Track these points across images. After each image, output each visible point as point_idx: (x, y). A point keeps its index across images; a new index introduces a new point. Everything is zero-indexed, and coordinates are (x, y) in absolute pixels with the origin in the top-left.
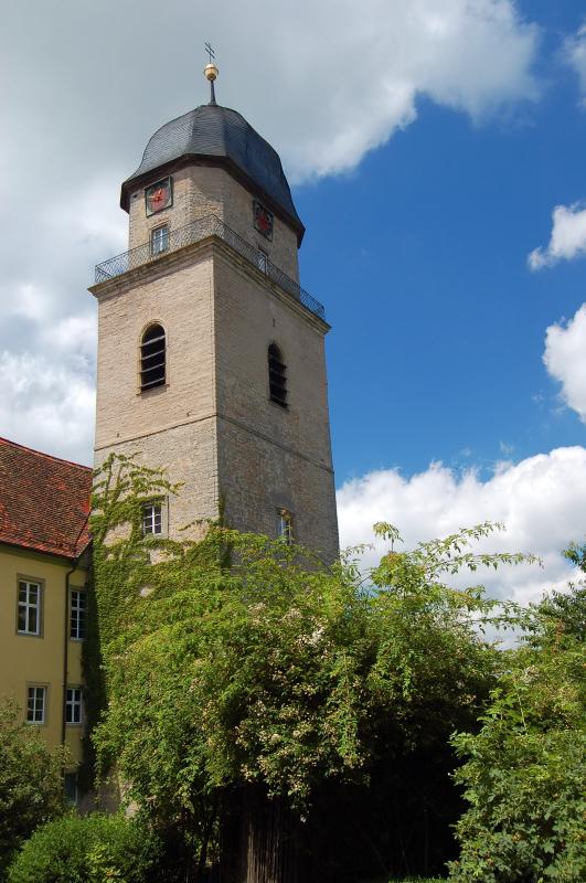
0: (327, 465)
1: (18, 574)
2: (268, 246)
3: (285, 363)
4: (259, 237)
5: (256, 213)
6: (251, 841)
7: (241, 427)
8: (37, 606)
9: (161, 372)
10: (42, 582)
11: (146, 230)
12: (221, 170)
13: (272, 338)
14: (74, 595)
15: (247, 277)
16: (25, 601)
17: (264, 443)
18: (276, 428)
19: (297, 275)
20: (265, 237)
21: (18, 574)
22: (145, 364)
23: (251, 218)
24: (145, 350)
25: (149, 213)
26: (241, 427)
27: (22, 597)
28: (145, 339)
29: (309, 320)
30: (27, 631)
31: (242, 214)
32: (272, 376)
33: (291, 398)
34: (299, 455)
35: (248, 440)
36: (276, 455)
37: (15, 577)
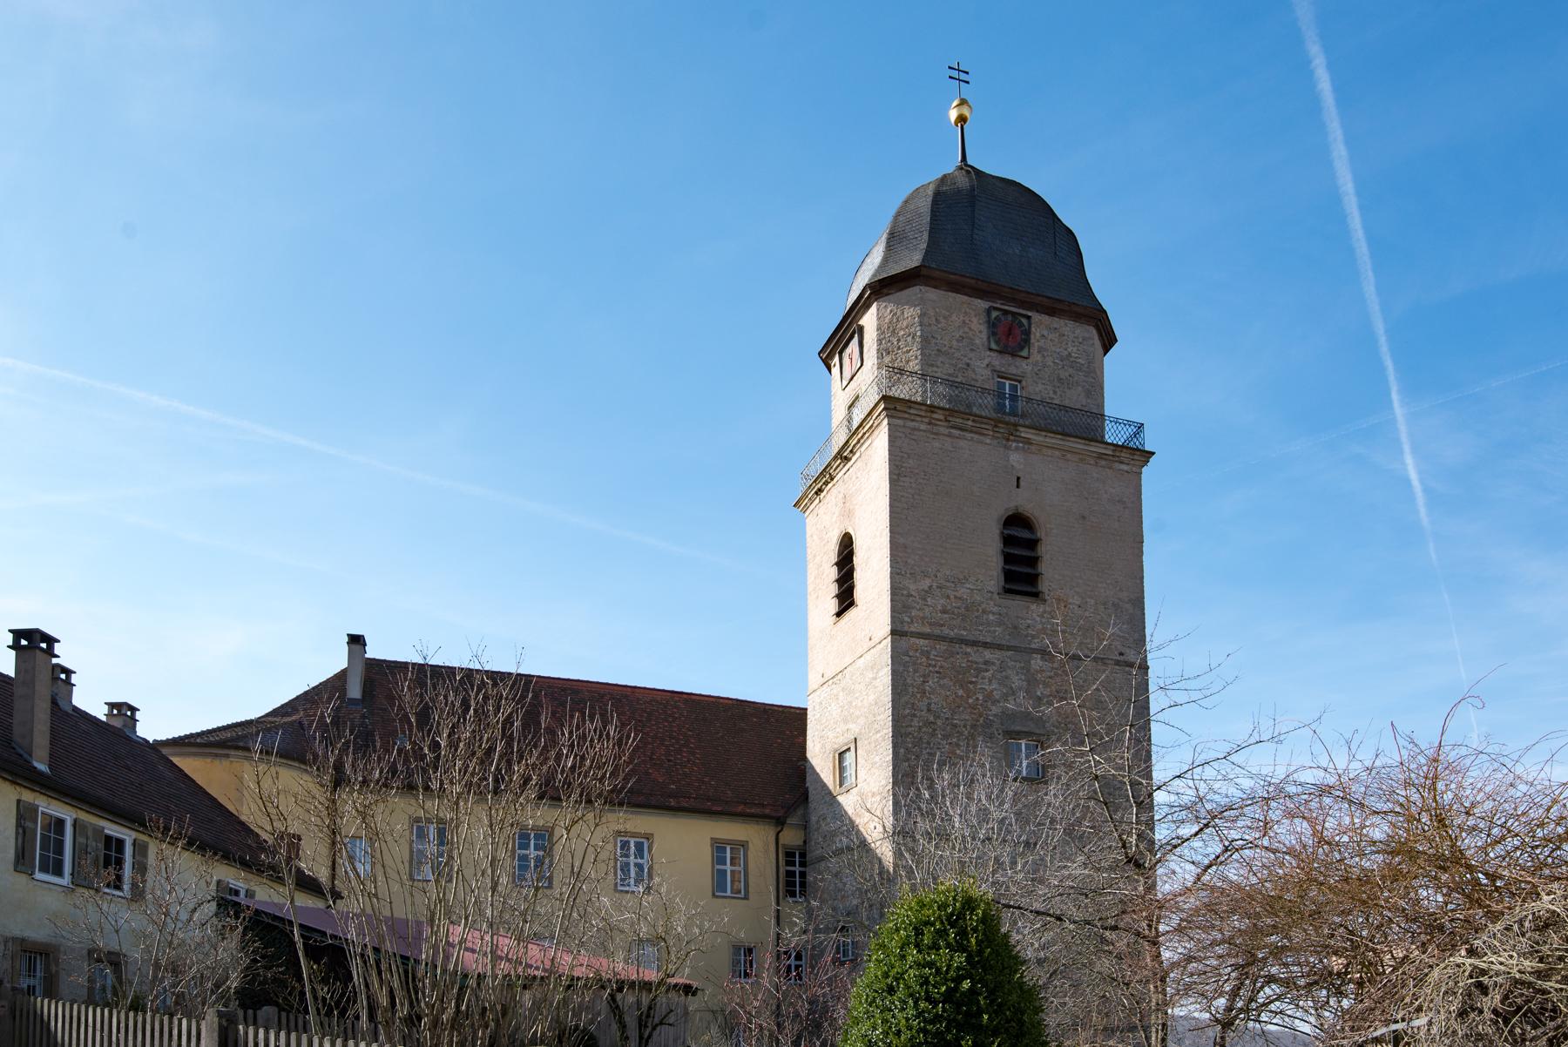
4: (998, 361)
12: (916, 289)
18: (1015, 627)
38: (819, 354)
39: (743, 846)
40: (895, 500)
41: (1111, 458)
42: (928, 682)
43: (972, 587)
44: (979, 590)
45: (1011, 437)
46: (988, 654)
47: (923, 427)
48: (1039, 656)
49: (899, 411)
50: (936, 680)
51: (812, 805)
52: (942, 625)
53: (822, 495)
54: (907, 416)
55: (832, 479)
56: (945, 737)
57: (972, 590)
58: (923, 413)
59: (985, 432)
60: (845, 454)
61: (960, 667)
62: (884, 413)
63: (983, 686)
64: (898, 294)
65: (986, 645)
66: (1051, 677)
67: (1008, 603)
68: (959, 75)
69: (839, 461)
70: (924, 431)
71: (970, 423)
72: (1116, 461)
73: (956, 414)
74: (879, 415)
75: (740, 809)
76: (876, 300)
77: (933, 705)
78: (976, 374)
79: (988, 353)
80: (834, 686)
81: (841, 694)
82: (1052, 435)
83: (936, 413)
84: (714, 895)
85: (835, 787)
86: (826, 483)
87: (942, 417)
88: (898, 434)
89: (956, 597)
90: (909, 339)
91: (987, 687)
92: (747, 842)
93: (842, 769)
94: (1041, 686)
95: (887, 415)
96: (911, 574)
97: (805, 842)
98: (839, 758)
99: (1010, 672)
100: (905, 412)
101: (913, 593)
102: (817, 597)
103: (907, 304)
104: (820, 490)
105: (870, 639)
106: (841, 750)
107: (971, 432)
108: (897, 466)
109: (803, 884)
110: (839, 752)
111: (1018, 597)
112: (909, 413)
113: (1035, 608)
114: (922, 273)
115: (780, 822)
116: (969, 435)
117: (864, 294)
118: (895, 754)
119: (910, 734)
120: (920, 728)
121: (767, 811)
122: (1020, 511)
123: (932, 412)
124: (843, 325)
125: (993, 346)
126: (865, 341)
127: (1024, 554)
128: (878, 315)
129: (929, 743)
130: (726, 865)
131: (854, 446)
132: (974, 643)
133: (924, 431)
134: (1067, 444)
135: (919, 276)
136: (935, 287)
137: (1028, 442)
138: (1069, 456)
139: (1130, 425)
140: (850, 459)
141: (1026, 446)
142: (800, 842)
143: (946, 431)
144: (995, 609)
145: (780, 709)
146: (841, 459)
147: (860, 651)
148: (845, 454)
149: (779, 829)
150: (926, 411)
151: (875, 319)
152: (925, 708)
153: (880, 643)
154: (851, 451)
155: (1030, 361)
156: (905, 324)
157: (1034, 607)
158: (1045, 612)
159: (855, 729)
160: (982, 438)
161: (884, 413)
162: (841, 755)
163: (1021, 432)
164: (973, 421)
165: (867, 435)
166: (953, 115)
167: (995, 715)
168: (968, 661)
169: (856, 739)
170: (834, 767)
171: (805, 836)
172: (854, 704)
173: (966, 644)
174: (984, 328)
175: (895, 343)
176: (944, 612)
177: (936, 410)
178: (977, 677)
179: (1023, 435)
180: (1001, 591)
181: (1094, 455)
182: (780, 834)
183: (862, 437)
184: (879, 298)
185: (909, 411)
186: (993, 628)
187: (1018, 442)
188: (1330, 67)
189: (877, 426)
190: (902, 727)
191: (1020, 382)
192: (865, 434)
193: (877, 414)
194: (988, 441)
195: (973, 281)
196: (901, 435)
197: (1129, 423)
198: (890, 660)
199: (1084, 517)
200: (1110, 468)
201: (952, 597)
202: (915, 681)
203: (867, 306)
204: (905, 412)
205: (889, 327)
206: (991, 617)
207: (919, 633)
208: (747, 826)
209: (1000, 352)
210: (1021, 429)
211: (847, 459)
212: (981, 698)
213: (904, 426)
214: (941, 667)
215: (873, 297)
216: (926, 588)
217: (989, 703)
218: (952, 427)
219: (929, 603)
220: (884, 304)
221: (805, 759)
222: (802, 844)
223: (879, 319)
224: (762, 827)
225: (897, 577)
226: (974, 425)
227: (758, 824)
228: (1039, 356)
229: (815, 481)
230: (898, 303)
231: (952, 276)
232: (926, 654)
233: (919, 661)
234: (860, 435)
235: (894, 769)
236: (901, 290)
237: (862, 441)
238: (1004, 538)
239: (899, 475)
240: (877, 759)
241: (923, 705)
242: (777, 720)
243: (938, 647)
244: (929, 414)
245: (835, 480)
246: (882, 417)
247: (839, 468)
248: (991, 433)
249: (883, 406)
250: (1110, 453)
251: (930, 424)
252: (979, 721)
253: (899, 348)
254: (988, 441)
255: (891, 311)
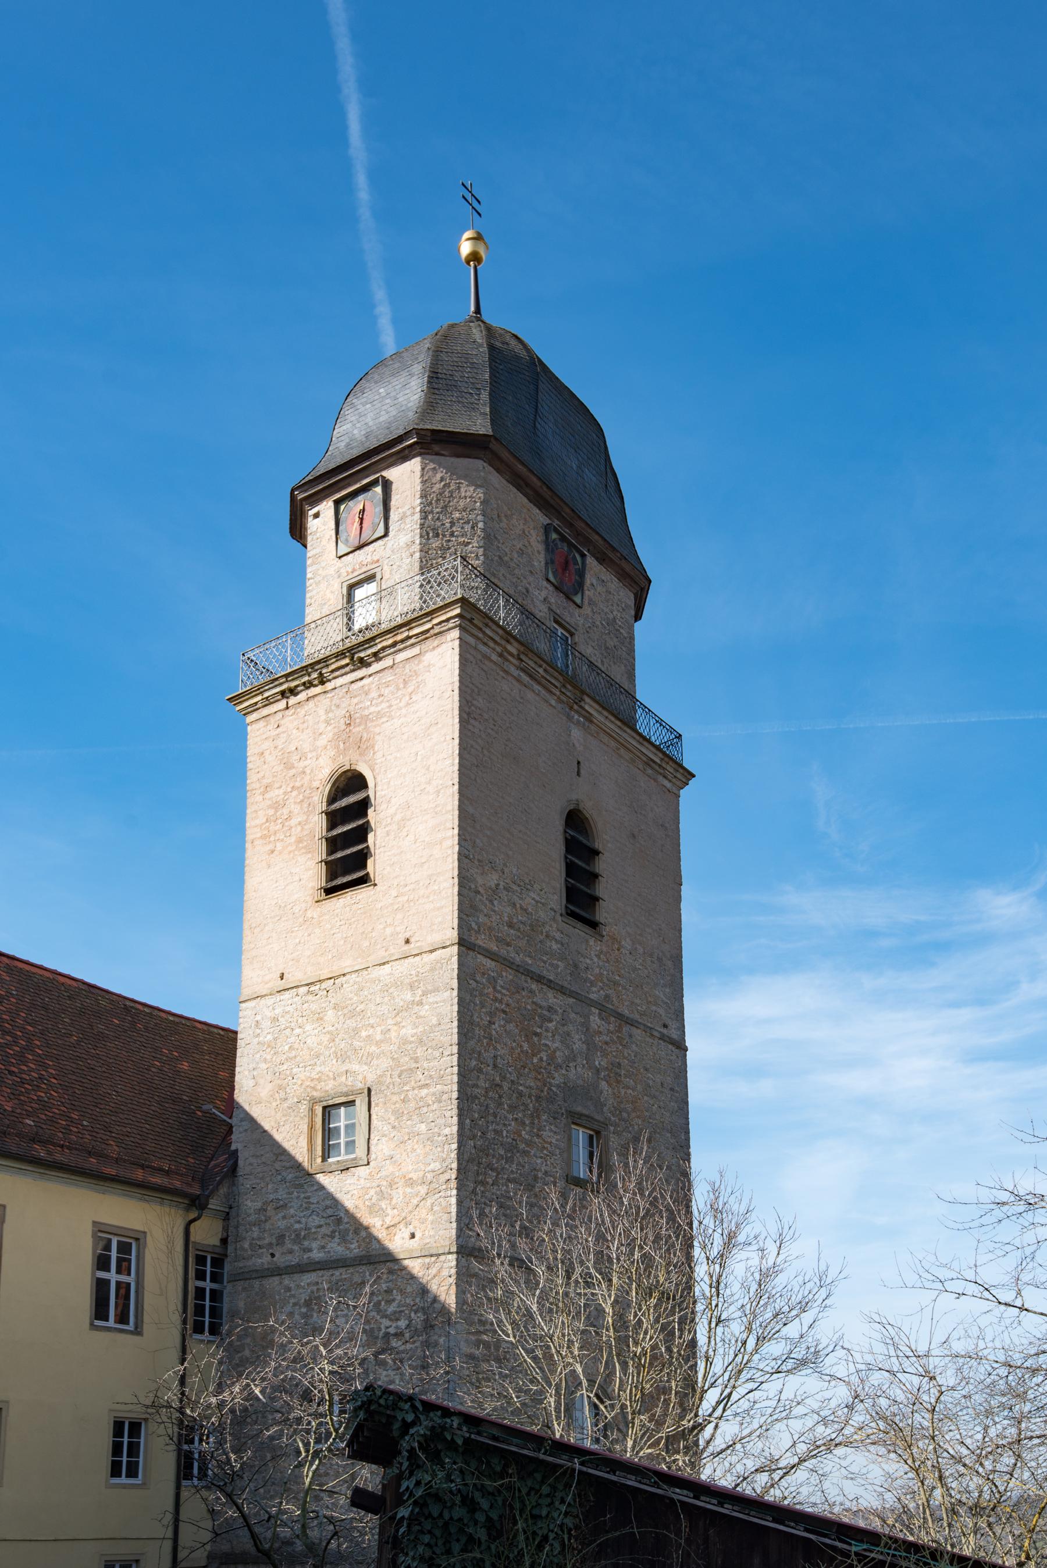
0: (674, 1035)
1: (94, 1222)
2: (574, 617)
3: (598, 845)
4: (556, 600)
5: (549, 547)
6: (380, 294)
7: (507, 963)
8: (131, 1279)
9: (361, 859)
10: (140, 1238)
11: (336, 585)
12: (479, 464)
13: (574, 797)
14: (201, 1260)
15: (525, 678)
16: (108, 1270)
17: (550, 994)
18: (576, 966)
19: (631, 676)
20: (568, 598)
21: (94, 1222)
22: (333, 844)
23: (539, 560)
24: (334, 818)
25: (343, 549)
26: (507, 963)
27: (102, 1263)
28: (332, 799)
29: (649, 762)
30: (111, 1323)
31: (521, 552)
32: (571, 870)
33: (603, 913)
34: (619, 1016)
35: (519, 989)
36: (573, 1015)
37: (89, 1229)
38: (293, 491)
39: (137, 1239)
40: (464, 749)
41: (657, 768)
42: (494, 1024)
43: (537, 898)
44: (543, 904)
45: (576, 707)
46: (552, 998)
47: (494, 657)
48: (597, 1011)
49: (476, 626)
50: (502, 1023)
51: (245, 1183)
52: (508, 944)
53: (293, 700)
54: (481, 635)
55: (322, 683)
56: (513, 1108)
57: (537, 902)
58: (497, 638)
59: (554, 690)
60: (362, 655)
61: (525, 1008)
62: (457, 621)
63: (547, 1042)
64: (453, 459)
65: (550, 984)
66: (606, 1043)
67: (569, 929)
68: (472, 200)
69: (347, 661)
70: (495, 663)
71: (541, 671)
72: (661, 774)
73: (530, 655)
74: (448, 620)
75: (139, 1175)
76: (420, 454)
77: (499, 1060)
78: (534, 606)
79: (545, 583)
80: (310, 997)
81: (330, 1013)
82: (613, 719)
83: (511, 644)
84: (92, 1324)
85: (312, 1159)
86: (308, 685)
87: (515, 652)
88: (468, 656)
89: (521, 908)
90: (468, 527)
91: (550, 1044)
92: (145, 1233)
93: (328, 1133)
94: (599, 1053)
95: (460, 626)
96: (479, 861)
97: (224, 1241)
98: (324, 1115)
99: (571, 1028)
100: (480, 629)
101: (481, 889)
102: (272, 852)
103: (465, 477)
104: (293, 692)
105: (407, 941)
106: (331, 1102)
107: (539, 683)
108: (467, 702)
109: (215, 1312)
110: (325, 1104)
111: (579, 925)
112: (484, 633)
113: (594, 946)
114: (491, 445)
115: (196, 1204)
116: (537, 687)
117: (407, 440)
118: (461, 1124)
119: (476, 1097)
120: (487, 1090)
121: (178, 1184)
122: (581, 808)
123: (508, 641)
124: (353, 467)
125: (551, 577)
126: (394, 503)
127: (345, 829)
128: (422, 476)
129: (495, 1115)
130: (109, 1271)
131: (383, 649)
132: (539, 979)
133: (495, 663)
134: (624, 735)
135: (486, 448)
136: (498, 471)
137: (589, 718)
138: (622, 751)
139: (671, 733)
140: (369, 665)
141: (587, 724)
142: (215, 1241)
143: (516, 673)
144: (558, 935)
145: (147, 1010)
146: (352, 659)
147: (381, 955)
148: (362, 655)
149: (193, 1215)
150: (502, 637)
151: (419, 481)
152: (491, 1062)
153: (431, 951)
154: (375, 654)
155: (581, 611)
156: (462, 504)
157: (592, 942)
158: (601, 952)
159: (363, 1074)
160: (548, 696)
161: (457, 621)
162: (328, 1111)
163: (585, 703)
164: (545, 670)
165: (413, 641)
166: (466, 248)
167: (558, 1086)
168: (533, 1002)
169: (369, 1090)
170: (311, 1127)
171: (226, 1229)
172: (364, 1034)
173: (532, 978)
174: (541, 547)
175: (448, 525)
176: (510, 925)
177: (512, 641)
178: (541, 1027)
179: (587, 707)
180: (564, 912)
181: (644, 759)
182: (192, 1225)
183: (402, 641)
184: (428, 454)
185: (484, 629)
186: (556, 962)
187: (580, 715)
188: (395, 321)
189: (435, 635)
190: (468, 1085)
191: (572, 634)
192: (409, 638)
193: (443, 618)
194: (553, 703)
195: (539, 484)
196: (472, 659)
197: (671, 730)
198: (456, 981)
199: (634, 836)
200: (655, 780)
201: (518, 906)
202: (481, 1019)
203: (403, 457)
204: (480, 629)
205: (438, 500)
206: (555, 946)
207: (487, 950)
208: (146, 1205)
209: (556, 588)
210: (587, 700)
211: (363, 663)
212: (545, 1058)
213: (475, 648)
214: (508, 1005)
215: (418, 450)
216: (493, 886)
217: (552, 1068)
218: (523, 670)
219: (497, 909)
220: (432, 466)
221: (231, 1105)
222: (218, 1243)
223: (423, 482)
224: (167, 1209)
225: (467, 861)
226: (545, 675)
227: (161, 1204)
228: (590, 609)
229: (287, 676)
230: (452, 471)
231: (520, 467)
232: (493, 981)
233: (486, 991)
234: (399, 637)
235: (459, 1148)
236: (458, 456)
237: (398, 647)
238: (566, 839)
239: (469, 714)
240: (423, 1127)
241: (488, 1055)
242: (146, 1029)
243: (504, 974)
244: (503, 642)
245: (329, 686)
246: (451, 625)
247: (343, 671)
248: (558, 693)
249: (458, 611)
250: (658, 761)
251: (501, 655)
252: (542, 1091)
253: (452, 535)
254: (553, 703)
255: (442, 479)
